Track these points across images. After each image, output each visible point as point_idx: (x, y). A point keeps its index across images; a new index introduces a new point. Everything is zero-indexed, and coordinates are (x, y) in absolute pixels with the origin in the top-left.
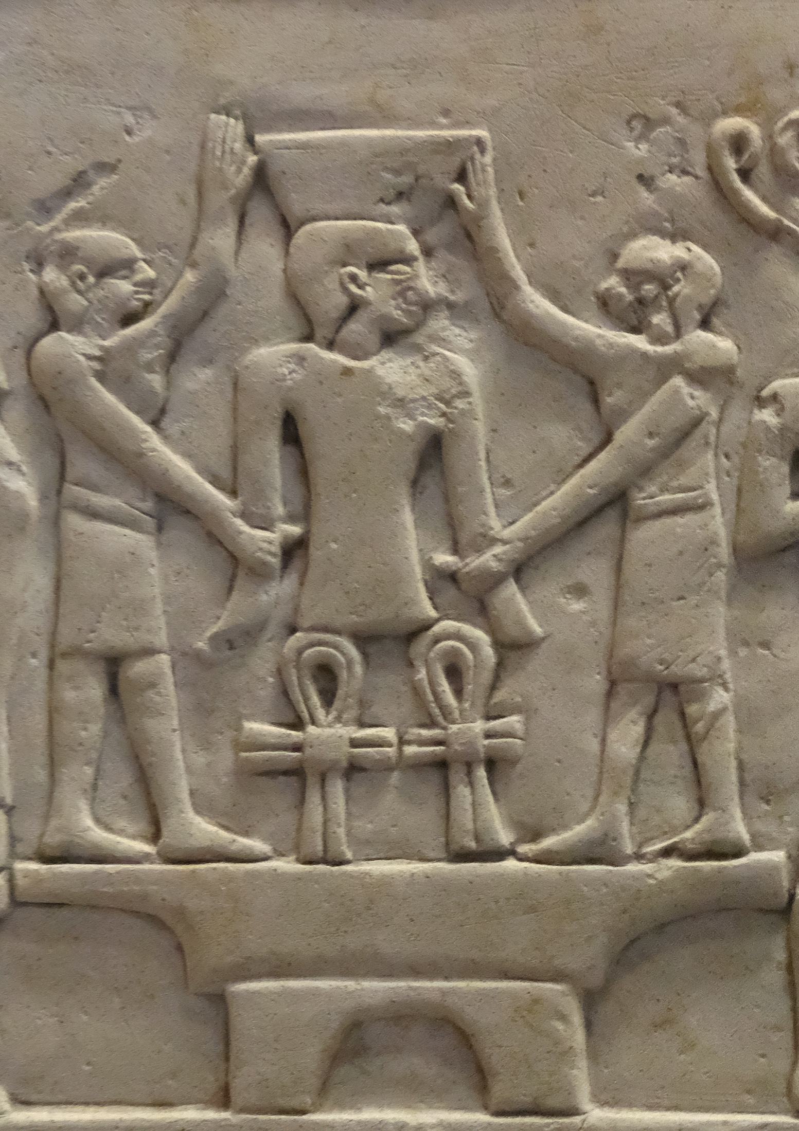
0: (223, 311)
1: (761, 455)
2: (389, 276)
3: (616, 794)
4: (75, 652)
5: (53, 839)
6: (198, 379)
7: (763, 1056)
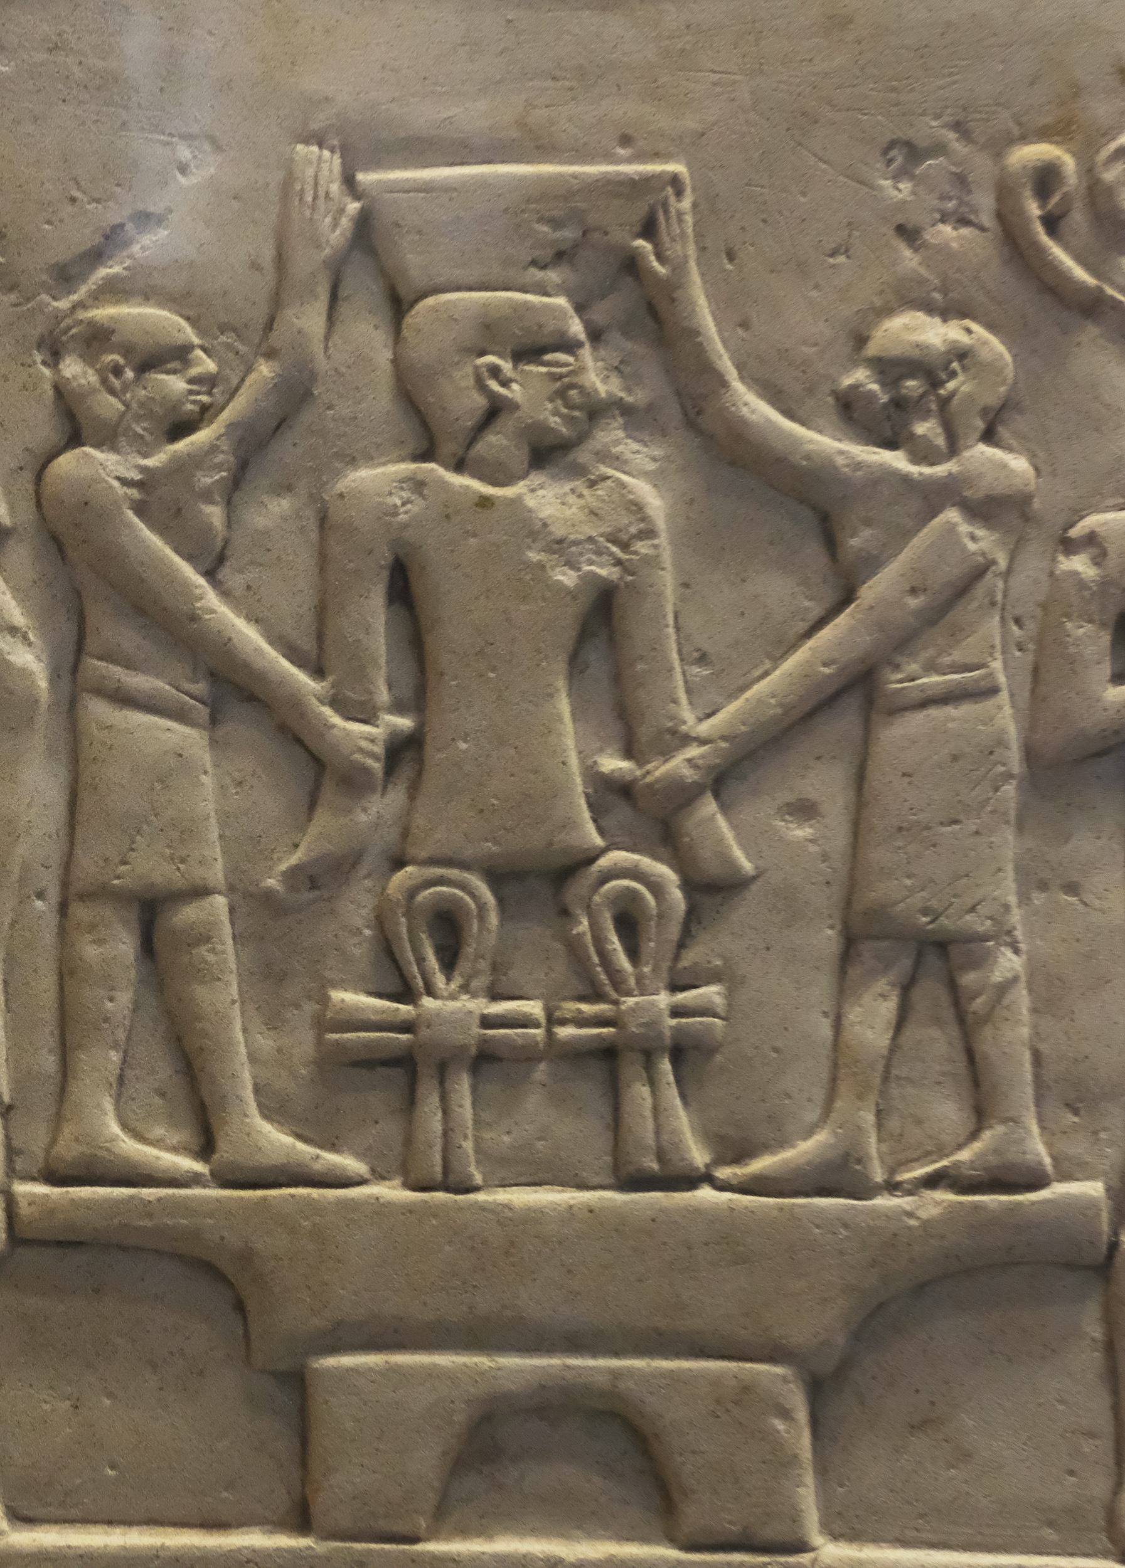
0: (307, 417)
1: (1070, 620)
2: (543, 369)
3: (860, 1097)
4: (100, 893)
5: (68, 1149)
6: (272, 512)
7: (1072, 1473)
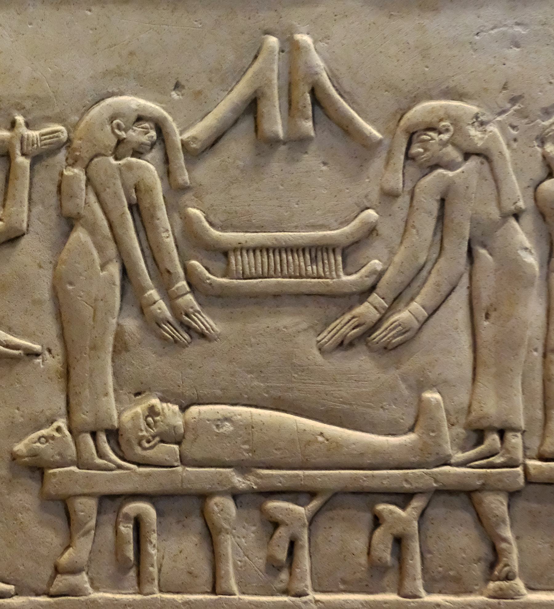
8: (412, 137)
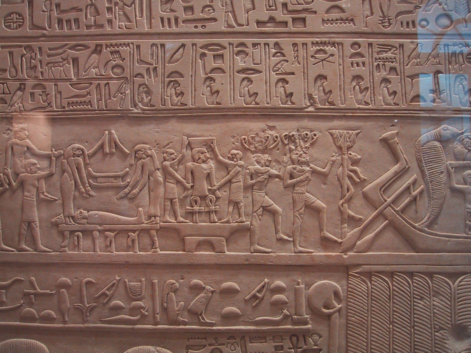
5: (165, 220)
6: (181, 167)
8: (136, 152)
